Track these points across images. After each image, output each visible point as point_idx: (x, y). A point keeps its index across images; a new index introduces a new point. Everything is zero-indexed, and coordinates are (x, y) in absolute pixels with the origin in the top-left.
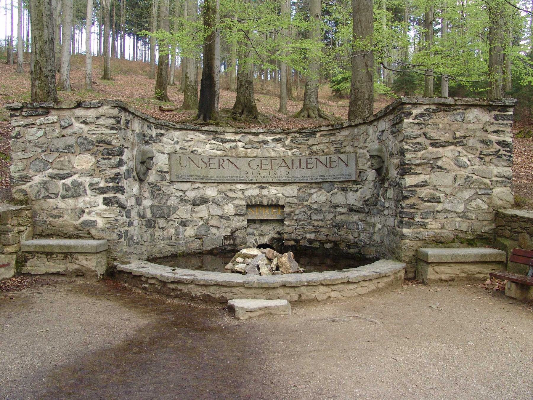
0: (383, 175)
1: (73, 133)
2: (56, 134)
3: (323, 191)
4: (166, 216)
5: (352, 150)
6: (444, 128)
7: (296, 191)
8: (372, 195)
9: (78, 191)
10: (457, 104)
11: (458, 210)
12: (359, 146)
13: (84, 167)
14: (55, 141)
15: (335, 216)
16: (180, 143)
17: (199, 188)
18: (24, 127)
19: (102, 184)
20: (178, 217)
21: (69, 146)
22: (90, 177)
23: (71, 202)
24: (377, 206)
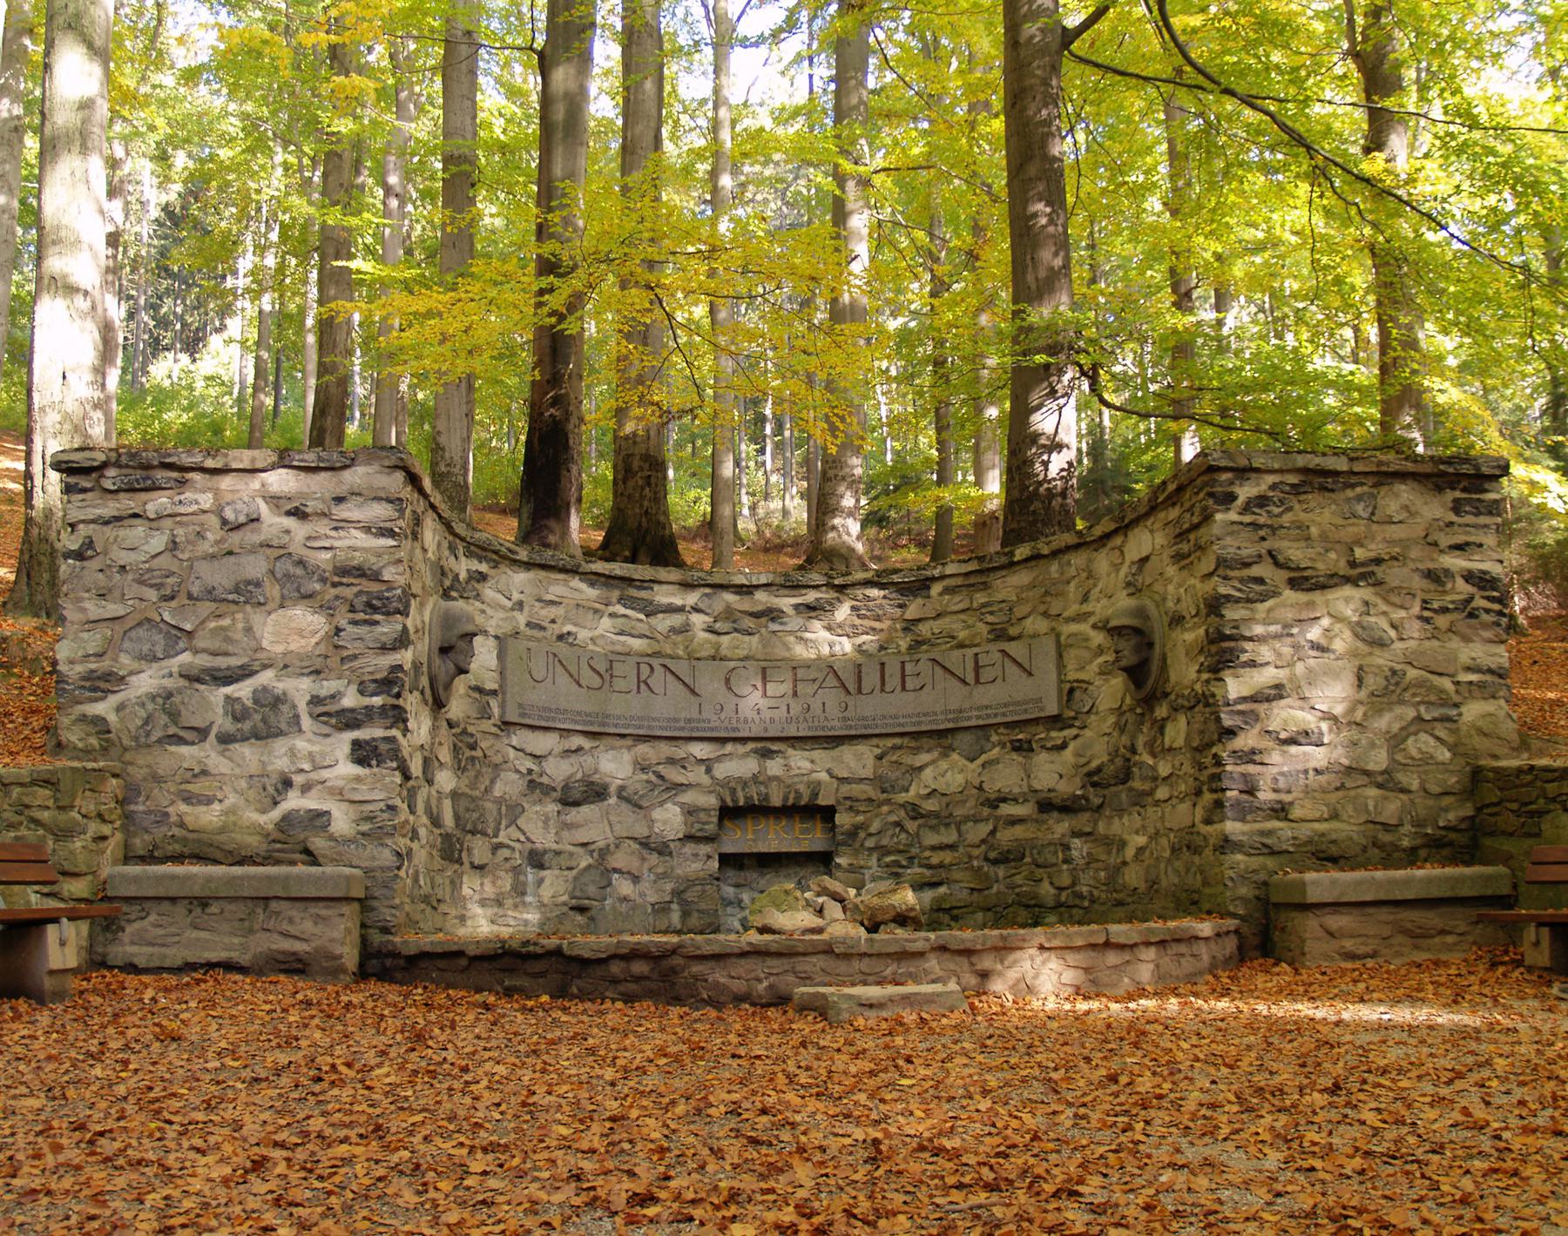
0: (1151, 681)
1: (261, 545)
2: (206, 547)
3: (955, 756)
4: (490, 831)
5: (1042, 625)
6: (1324, 537)
7: (870, 761)
8: (1114, 754)
9: (272, 719)
10: (1356, 469)
11: (1371, 767)
12: (1066, 614)
13: (293, 647)
14: (203, 568)
15: (993, 832)
16: (526, 609)
17: (579, 749)
18: (106, 523)
19: (350, 700)
20: (522, 838)
21: (249, 583)
22: (312, 678)
23: (247, 752)
24: (1130, 783)
